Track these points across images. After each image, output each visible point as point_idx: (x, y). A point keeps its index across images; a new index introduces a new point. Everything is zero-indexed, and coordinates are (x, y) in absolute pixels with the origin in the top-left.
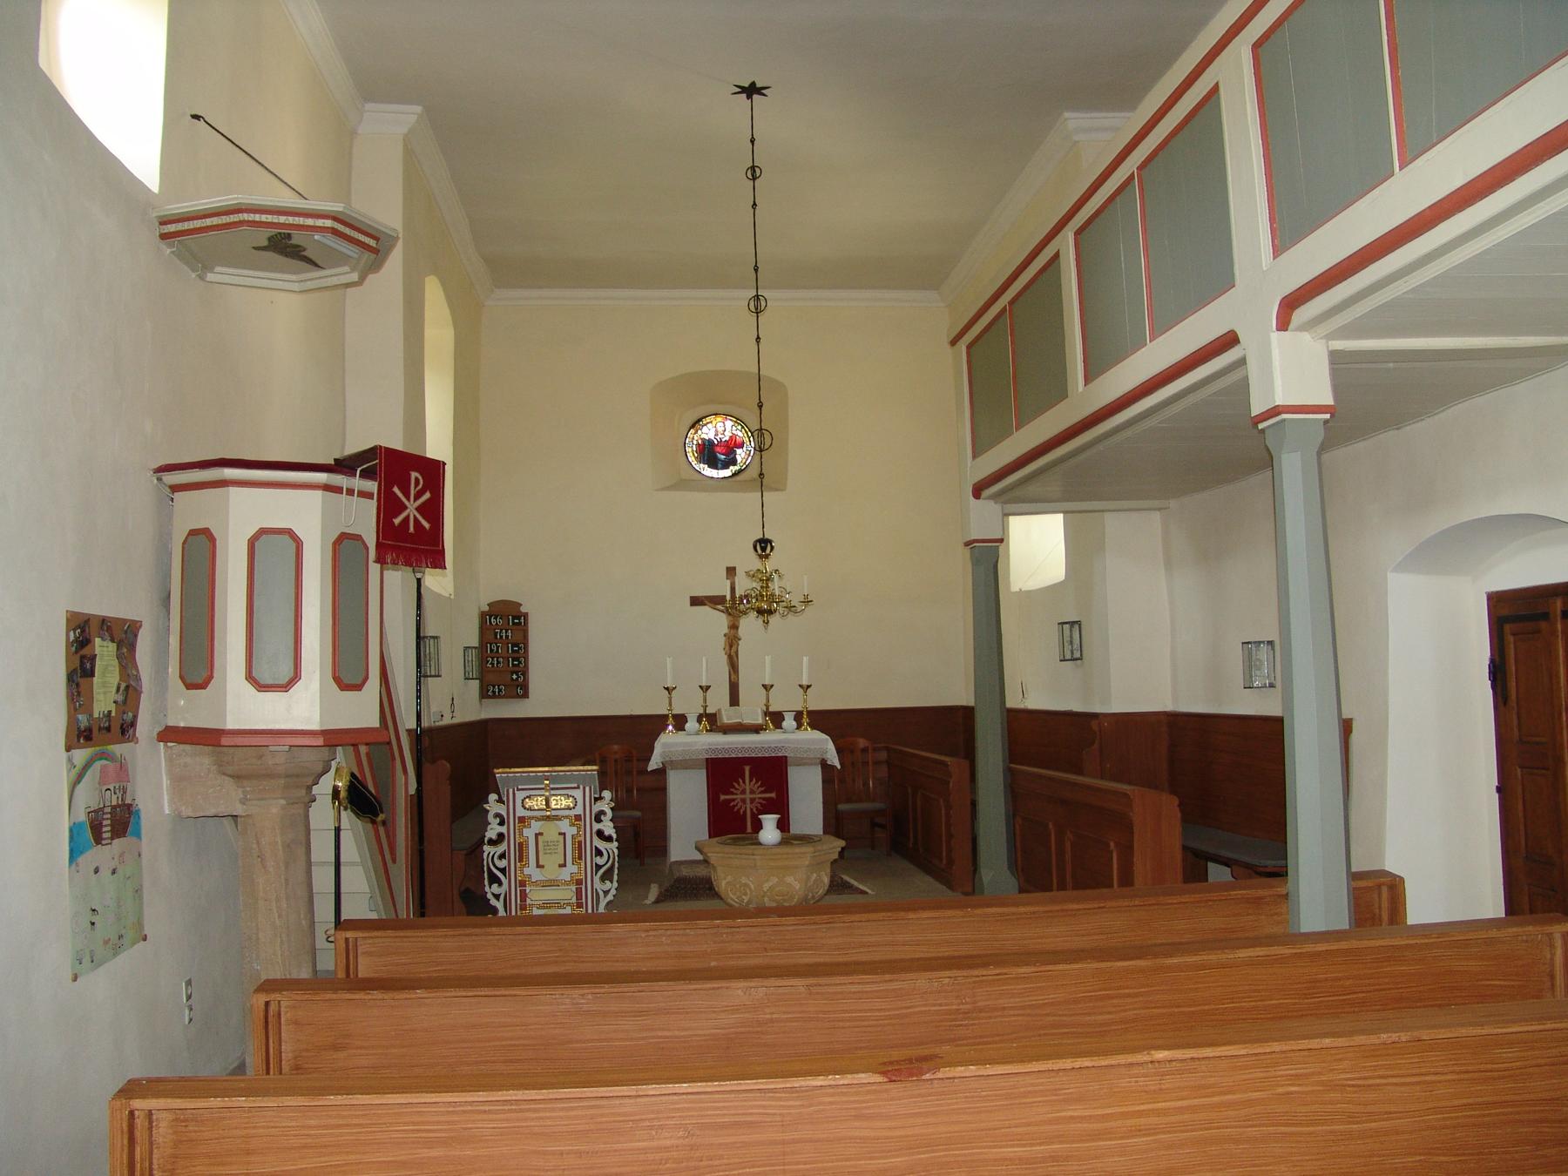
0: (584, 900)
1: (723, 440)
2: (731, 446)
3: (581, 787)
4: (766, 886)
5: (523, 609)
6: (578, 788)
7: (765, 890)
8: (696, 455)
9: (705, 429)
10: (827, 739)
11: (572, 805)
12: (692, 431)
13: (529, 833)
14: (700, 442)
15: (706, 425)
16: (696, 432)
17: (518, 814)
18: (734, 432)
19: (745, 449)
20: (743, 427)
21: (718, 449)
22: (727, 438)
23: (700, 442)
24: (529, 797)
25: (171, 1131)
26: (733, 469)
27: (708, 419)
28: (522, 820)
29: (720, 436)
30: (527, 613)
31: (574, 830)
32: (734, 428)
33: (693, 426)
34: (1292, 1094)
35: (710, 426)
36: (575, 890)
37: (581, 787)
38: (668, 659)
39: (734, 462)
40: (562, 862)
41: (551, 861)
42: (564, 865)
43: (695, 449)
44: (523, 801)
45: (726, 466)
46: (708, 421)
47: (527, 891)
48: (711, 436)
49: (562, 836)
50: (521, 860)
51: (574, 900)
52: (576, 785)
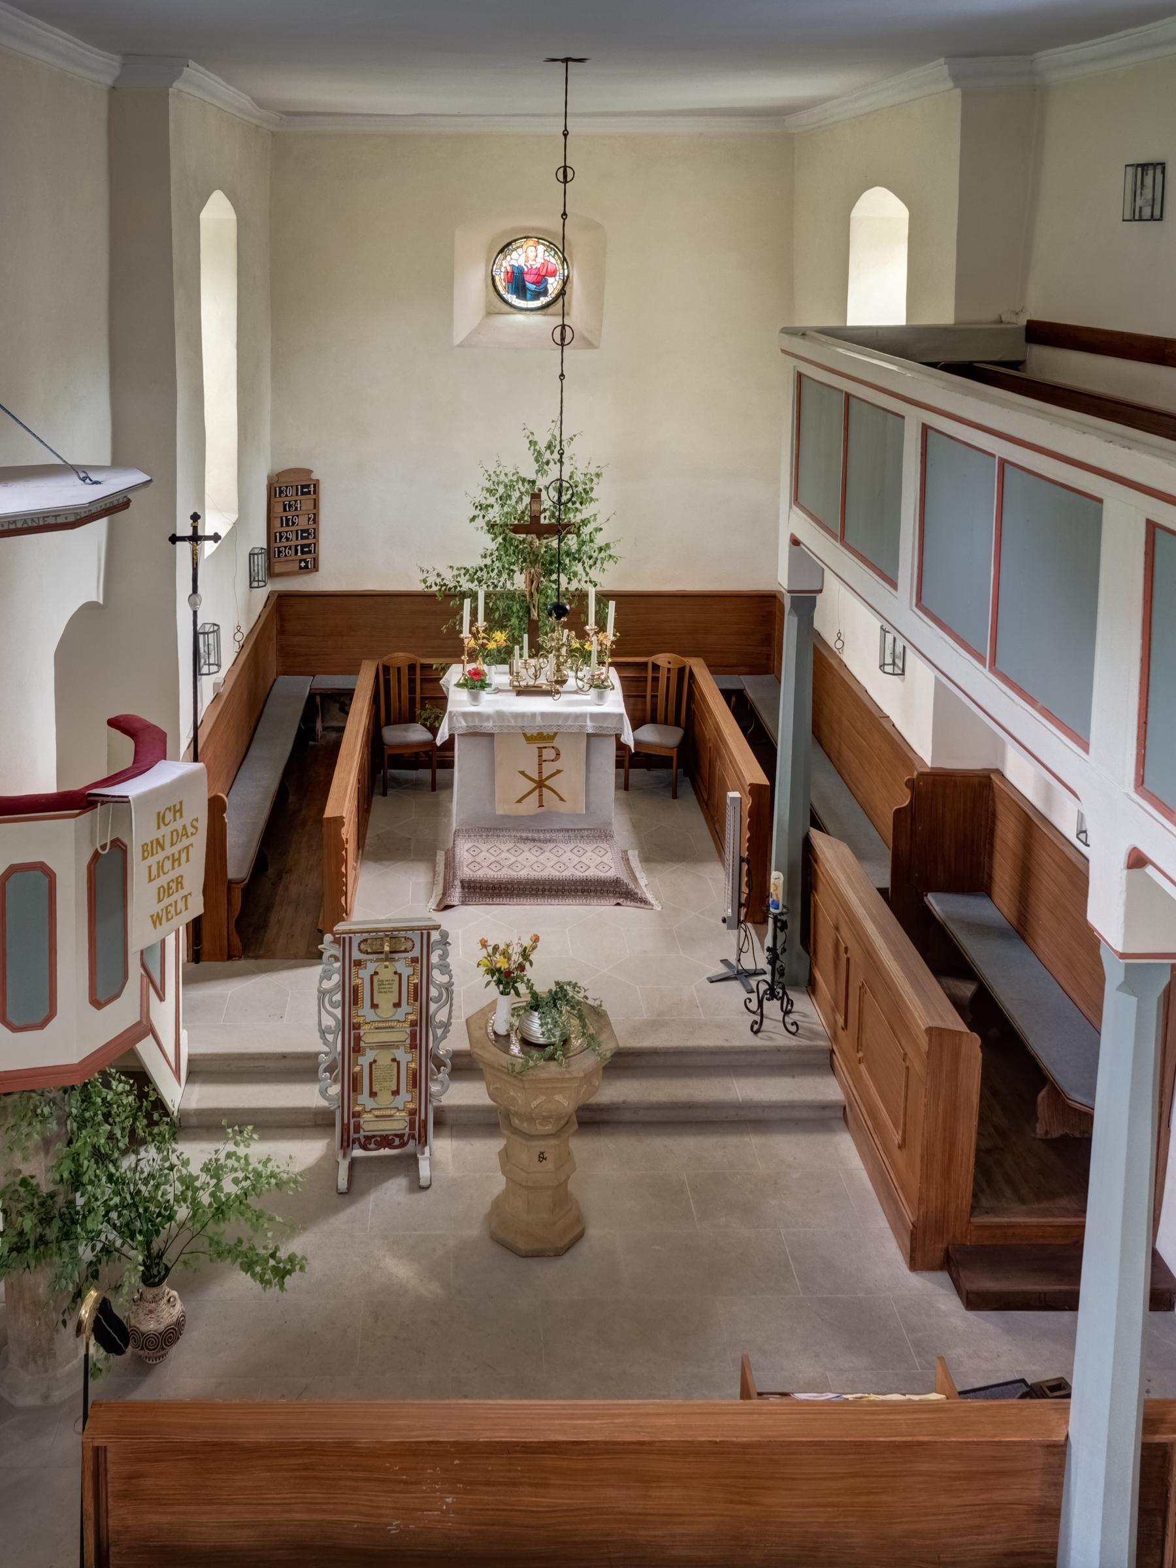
1: (534, 267)
2: (541, 278)
4: (534, 1104)
5: (314, 476)
7: (533, 1107)
8: (504, 284)
13: (365, 974)
14: (509, 269)
15: (515, 250)
16: (505, 258)
17: (353, 958)
18: (547, 258)
19: (557, 278)
20: (556, 253)
21: (527, 277)
22: (538, 265)
23: (509, 269)
24: (365, 940)
25: (43, 1261)
26: (543, 300)
27: (518, 243)
28: (358, 963)
29: (531, 262)
30: (318, 481)
31: (410, 971)
32: (547, 254)
33: (502, 251)
35: (520, 250)
39: (545, 293)
40: (397, 1001)
41: (385, 1001)
42: (397, 1005)
43: (502, 278)
45: (537, 295)
46: (518, 245)
47: (362, 1123)
48: (521, 262)
49: (397, 976)
50: (355, 1090)
51: (408, 1042)
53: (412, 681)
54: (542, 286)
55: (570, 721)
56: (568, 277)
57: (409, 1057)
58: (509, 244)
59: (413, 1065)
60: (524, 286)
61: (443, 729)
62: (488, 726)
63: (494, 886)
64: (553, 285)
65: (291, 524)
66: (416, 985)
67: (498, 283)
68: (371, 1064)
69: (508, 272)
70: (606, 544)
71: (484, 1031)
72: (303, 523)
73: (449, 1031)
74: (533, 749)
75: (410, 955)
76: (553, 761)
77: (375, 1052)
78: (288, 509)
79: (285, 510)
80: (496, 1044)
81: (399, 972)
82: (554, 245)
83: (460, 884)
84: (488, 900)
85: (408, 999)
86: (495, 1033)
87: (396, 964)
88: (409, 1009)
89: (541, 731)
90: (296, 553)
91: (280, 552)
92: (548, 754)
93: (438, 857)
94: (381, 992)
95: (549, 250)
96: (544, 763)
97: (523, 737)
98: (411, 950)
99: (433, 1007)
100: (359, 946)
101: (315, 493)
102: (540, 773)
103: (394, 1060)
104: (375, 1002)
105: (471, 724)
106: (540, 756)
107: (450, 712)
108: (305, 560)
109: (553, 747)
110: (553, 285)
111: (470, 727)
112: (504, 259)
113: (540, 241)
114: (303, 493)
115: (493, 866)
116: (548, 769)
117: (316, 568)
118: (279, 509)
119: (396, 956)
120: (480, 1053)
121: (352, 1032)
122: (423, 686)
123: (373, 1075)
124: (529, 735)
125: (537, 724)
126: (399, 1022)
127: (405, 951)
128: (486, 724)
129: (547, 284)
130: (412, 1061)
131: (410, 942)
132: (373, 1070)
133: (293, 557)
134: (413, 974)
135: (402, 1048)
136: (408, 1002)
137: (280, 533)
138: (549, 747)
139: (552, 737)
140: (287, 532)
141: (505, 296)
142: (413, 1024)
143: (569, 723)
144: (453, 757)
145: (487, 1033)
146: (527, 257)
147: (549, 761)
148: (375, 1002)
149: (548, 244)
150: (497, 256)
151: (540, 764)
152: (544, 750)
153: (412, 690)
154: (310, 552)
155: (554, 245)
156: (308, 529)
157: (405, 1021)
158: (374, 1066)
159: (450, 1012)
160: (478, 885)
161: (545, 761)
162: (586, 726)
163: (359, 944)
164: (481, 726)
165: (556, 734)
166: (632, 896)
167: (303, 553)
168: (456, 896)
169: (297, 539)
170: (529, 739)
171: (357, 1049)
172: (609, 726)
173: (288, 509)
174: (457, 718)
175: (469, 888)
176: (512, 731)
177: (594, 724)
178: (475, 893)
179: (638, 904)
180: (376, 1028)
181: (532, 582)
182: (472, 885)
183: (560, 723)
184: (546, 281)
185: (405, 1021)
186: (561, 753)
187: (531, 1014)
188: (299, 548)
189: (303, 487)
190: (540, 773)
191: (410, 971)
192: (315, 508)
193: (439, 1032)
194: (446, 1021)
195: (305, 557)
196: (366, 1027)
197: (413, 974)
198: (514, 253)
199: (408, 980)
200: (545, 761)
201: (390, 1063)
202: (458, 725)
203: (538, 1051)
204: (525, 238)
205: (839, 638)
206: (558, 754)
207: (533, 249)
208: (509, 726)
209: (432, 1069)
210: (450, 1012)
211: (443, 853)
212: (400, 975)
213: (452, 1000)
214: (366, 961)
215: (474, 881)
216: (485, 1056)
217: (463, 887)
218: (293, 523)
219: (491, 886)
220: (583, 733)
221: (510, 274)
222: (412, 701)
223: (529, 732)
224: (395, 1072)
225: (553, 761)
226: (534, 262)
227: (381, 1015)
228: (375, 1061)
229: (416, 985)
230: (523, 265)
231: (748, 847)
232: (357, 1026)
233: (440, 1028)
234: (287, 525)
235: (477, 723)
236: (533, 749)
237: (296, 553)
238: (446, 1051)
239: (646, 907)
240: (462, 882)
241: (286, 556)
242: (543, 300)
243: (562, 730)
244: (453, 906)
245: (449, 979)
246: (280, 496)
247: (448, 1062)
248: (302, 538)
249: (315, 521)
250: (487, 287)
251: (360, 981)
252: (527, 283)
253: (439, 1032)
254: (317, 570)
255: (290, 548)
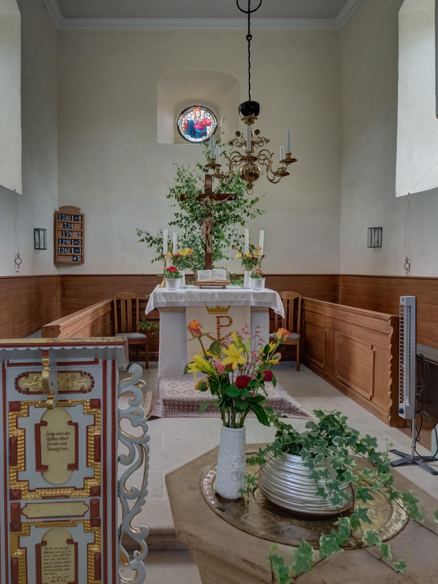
0: (101, 516)
1: (199, 121)
2: (204, 125)
3: (100, 361)
5: (82, 212)
6: (96, 362)
8: (184, 130)
9: (189, 115)
10: (275, 294)
11: (86, 387)
12: (182, 116)
14: (186, 122)
15: (189, 112)
16: (184, 117)
18: (206, 117)
19: (211, 127)
21: (196, 126)
24: (26, 375)
26: (204, 138)
27: (191, 109)
29: (197, 119)
30: (83, 214)
31: (90, 420)
33: (182, 113)
34: (353, 390)
36: (88, 503)
37: (100, 361)
38: (174, 233)
39: (205, 134)
40: (73, 462)
42: (73, 467)
43: (183, 126)
44: (92, 386)
45: (201, 136)
46: (191, 110)
47: (22, 506)
48: (193, 118)
49: (73, 428)
51: (88, 516)
52: (92, 359)
53: (134, 310)
54: (203, 131)
55: (239, 298)
56: (217, 126)
57: (90, 537)
58: (186, 109)
59: (95, 549)
60: (195, 131)
61: (150, 303)
62: (182, 302)
63: (188, 404)
64: (209, 130)
65: (68, 236)
66: (97, 439)
67: (181, 129)
68: (38, 547)
69: (186, 124)
70: (256, 199)
71: (198, 492)
72: (75, 236)
73: (144, 503)
74: (213, 317)
75: (87, 397)
76: (227, 326)
77: (43, 531)
78: (66, 227)
79: (64, 227)
80: (223, 514)
81: (74, 421)
82: (210, 110)
83: (162, 402)
84: (184, 414)
85: (87, 459)
86: (217, 496)
87: (71, 410)
88: (89, 472)
89: (219, 305)
90: (71, 252)
91: (61, 250)
92: (224, 321)
93: (147, 394)
94: (51, 450)
95: (207, 112)
96: (221, 328)
97: (206, 309)
98: (90, 390)
99: (121, 469)
100: (16, 383)
101: (82, 221)
102: (219, 334)
103: (70, 541)
104: (43, 463)
105: (169, 301)
106: (218, 323)
107: (155, 293)
108: (76, 256)
109: (227, 317)
110: (209, 130)
111: (169, 303)
112: (183, 117)
113: (202, 108)
114: (75, 220)
115: (187, 392)
116: (224, 332)
117: (82, 261)
118: (61, 227)
119: (70, 398)
120: (194, 532)
121: (9, 502)
122: (141, 313)
123: (43, 562)
124: (210, 308)
125: (216, 300)
126: (76, 489)
127: (83, 391)
128: (180, 301)
129: (206, 129)
130: (94, 543)
131: (89, 381)
132: (43, 555)
133: (69, 254)
134: (94, 425)
135: (80, 526)
136: (87, 462)
137: (62, 239)
138: (224, 317)
139: (226, 310)
140: (65, 239)
141: (184, 136)
142: (94, 492)
143: (238, 299)
144: (158, 355)
145: (204, 496)
146: (196, 116)
147: (225, 326)
148: (43, 463)
149: (206, 109)
150: (180, 116)
151: (218, 329)
152: (221, 319)
153: (134, 315)
154: (79, 252)
155: (210, 110)
156: (78, 240)
157: (83, 489)
158: (43, 549)
159: (145, 475)
160: (176, 403)
161: (222, 326)
162: (250, 301)
163: (17, 380)
164: (176, 302)
165: (229, 307)
166: (294, 411)
167: (75, 252)
168: (160, 410)
169: (71, 244)
170: (211, 311)
171: (16, 526)
172: (267, 301)
173: (66, 227)
174: (159, 297)
175: (170, 405)
176: (199, 305)
177: (255, 300)
178: (174, 409)
179: (300, 417)
180: (43, 498)
181: (208, 229)
182: (172, 403)
183: (232, 300)
184: (206, 128)
185: (83, 489)
186: (233, 321)
187: (285, 459)
188: (73, 249)
189: (75, 216)
190: (219, 334)
191: (90, 420)
192: (82, 229)
193: (131, 503)
194: (140, 489)
195: (76, 254)
196: (29, 496)
197: (94, 425)
198: (189, 114)
199: (87, 432)
200: (222, 326)
201: (65, 545)
202: (160, 301)
203: (307, 527)
204: (194, 106)
205: (407, 262)
206: (231, 322)
207: (198, 112)
208: (196, 302)
209: (121, 553)
210: (145, 475)
211: (151, 392)
212: (76, 425)
213: (147, 459)
214: (28, 404)
215: (174, 401)
216: (205, 538)
217: (165, 404)
218: (69, 236)
219: (186, 404)
220: (249, 306)
221: (187, 125)
222: (134, 321)
223: (210, 306)
224: (72, 558)
225: (227, 326)
226: (199, 119)
227: (52, 480)
228: (44, 543)
229: (97, 439)
230: (193, 120)
231: (391, 367)
232: (15, 494)
233: (132, 498)
234: (66, 235)
235: (174, 300)
236: (213, 317)
237: (71, 252)
238: (141, 529)
239: (307, 418)
240: (164, 401)
241: (65, 252)
242: (204, 138)
243: (234, 305)
244: (157, 418)
245: (142, 433)
246: (61, 219)
247: (144, 544)
248: (75, 244)
249: (81, 236)
250: (175, 130)
251: (20, 432)
252: (196, 129)
253: (131, 503)
254: (83, 263)
255: (67, 249)
